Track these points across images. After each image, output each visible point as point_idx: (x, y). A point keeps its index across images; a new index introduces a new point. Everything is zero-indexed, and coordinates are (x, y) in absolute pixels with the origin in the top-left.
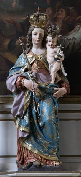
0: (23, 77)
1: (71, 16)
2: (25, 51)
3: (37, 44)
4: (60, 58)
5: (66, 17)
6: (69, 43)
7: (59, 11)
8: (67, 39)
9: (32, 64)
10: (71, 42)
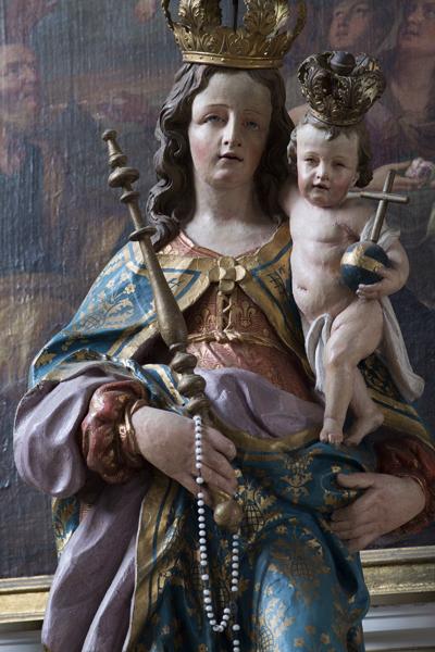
7: (415, 8)
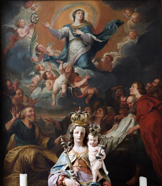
0: (64, 176)
1: (109, 115)
2: (67, 149)
3: (78, 142)
4: (101, 157)
5: (104, 116)
6: (107, 141)
8: (105, 137)
9: (73, 163)
10: (109, 140)
